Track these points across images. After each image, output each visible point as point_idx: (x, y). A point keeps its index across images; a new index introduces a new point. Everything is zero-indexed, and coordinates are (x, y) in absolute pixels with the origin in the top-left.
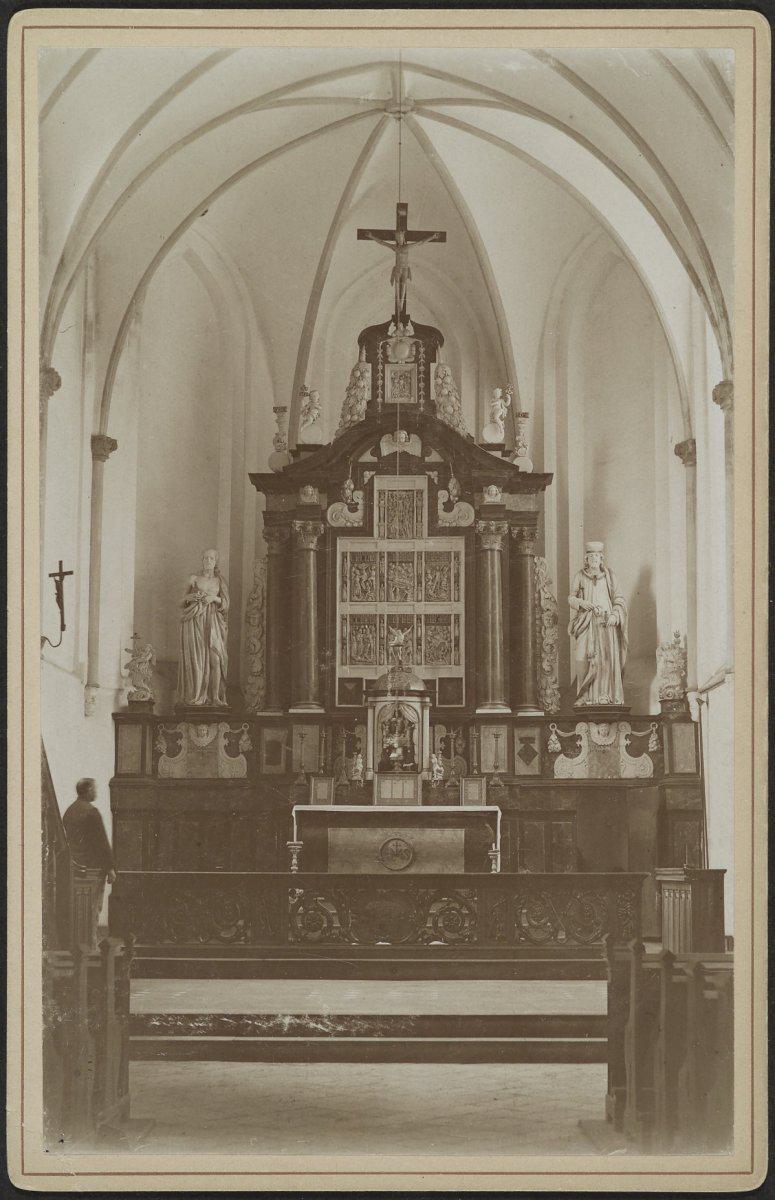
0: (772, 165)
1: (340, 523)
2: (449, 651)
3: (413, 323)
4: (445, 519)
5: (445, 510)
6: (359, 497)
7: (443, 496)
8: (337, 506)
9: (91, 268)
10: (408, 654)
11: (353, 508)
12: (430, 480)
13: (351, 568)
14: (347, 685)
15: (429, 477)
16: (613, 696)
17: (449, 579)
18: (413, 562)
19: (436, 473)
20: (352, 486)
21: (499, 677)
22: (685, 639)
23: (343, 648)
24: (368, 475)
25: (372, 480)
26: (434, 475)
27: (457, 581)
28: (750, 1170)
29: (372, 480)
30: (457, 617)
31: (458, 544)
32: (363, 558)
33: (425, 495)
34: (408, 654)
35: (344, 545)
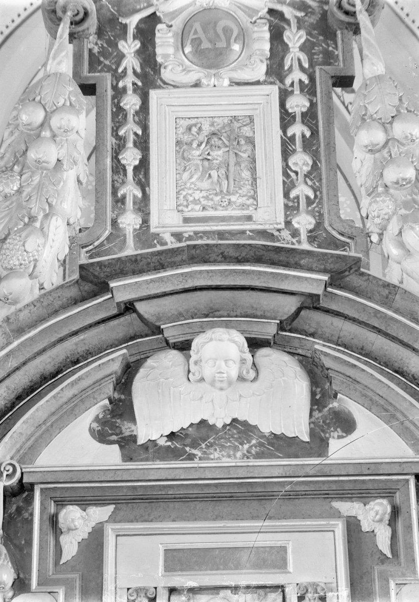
12: (353, 527)
24: (78, 521)
26: (372, 515)
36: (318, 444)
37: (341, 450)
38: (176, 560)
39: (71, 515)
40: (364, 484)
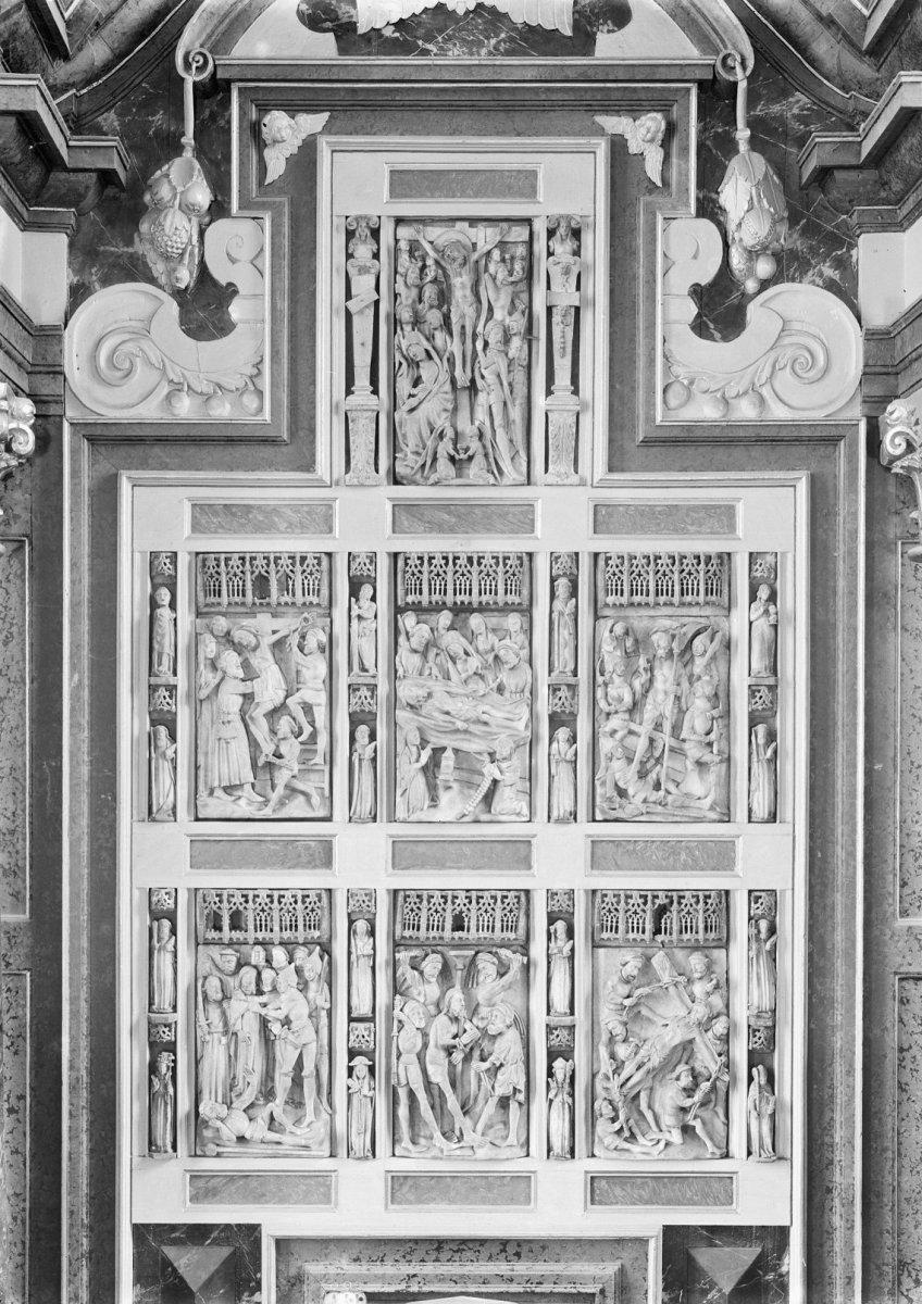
0: (896, 116)
1: (129, 402)
2: (719, 1098)
3: (350, 1061)
4: (702, 379)
5: (700, 328)
6: (241, 250)
7: (686, 252)
8: (117, 302)
9: (888, 1232)
11: (205, 307)
12: (620, 158)
15: (618, 146)
17: (721, 698)
18: (527, 611)
20: (202, 196)
24: (286, 130)
25: (305, 162)
26: (642, 132)
29: (305, 162)
31: (769, 516)
32: (262, 583)
33: (597, 245)
34: (504, 1103)
36: (583, 39)
37: (610, 46)
38: (402, 183)
39: (278, 122)
40: (636, 90)
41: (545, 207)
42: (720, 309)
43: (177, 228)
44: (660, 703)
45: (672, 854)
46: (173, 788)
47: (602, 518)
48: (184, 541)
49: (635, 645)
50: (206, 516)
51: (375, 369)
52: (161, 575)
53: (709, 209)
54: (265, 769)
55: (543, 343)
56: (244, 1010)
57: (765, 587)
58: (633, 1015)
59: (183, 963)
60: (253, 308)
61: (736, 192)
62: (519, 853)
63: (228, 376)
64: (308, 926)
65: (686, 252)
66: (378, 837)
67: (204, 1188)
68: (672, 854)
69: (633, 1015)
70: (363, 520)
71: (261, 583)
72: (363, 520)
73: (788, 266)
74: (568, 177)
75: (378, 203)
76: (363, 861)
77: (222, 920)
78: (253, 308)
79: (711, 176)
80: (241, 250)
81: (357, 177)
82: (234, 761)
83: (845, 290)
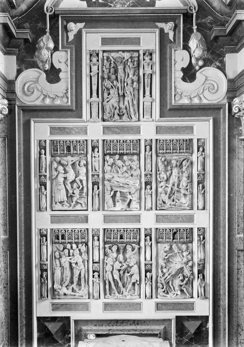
2: (190, 282)
4: (185, 93)
5: (184, 79)
6: (62, 59)
7: (180, 59)
8: (30, 74)
10: (134, 284)
11: (53, 75)
12: (163, 35)
13: (51, 163)
14: (47, 324)
15: (162, 31)
16: (60, 261)
17: (190, 177)
18: (139, 155)
19: (171, 24)
20: (51, 45)
21: (23, 244)
22: (166, 296)
23: (42, 276)
24: (74, 27)
25: (79, 36)
26: (168, 27)
27: (201, 182)
28: (66, 63)
29: (79, 36)
30: (202, 232)
32: (69, 148)
33: (156, 57)
34: (134, 284)
35: (41, 130)
39: (71, 25)
41: (142, 47)
42: (189, 74)
43: (45, 54)
44: (174, 179)
45: (177, 219)
46: (45, 202)
47: (159, 130)
48: (48, 137)
49: (168, 163)
50: (53, 130)
51: (101, 91)
52: (42, 146)
53: (186, 47)
54: (70, 197)
55: (142, 83)
56: (65, 260)
57: (202, 147)
58: (168, 261)
59: (49, 249)
60: (65, 75)
61: (193, 43)
62: (137, 219)
63: (59, 93)
64: (82, 239)
65: (180, 59)
66: (100, 215)
67: (55, 307)
68: (177, 219)
69: (168, 261)
70: (95, 131)
71: (68, 148)
72: (95, 131)
73: (207, 63)
74: (149, 40)
75: (98, 47)
76: (96, 221)
77: (59, 237)
78: (65, 75)
79: (186, 39)
80: (62, 59)
81: (93, 40)
82: (62, 195)
83: (222, 68)
